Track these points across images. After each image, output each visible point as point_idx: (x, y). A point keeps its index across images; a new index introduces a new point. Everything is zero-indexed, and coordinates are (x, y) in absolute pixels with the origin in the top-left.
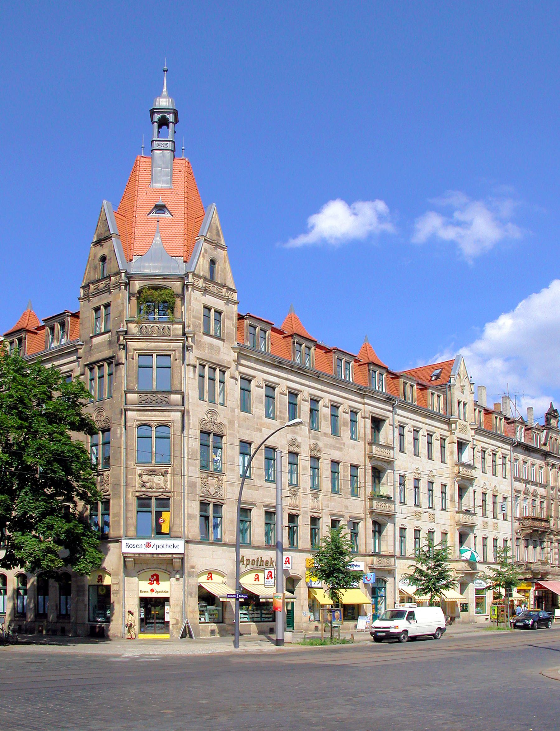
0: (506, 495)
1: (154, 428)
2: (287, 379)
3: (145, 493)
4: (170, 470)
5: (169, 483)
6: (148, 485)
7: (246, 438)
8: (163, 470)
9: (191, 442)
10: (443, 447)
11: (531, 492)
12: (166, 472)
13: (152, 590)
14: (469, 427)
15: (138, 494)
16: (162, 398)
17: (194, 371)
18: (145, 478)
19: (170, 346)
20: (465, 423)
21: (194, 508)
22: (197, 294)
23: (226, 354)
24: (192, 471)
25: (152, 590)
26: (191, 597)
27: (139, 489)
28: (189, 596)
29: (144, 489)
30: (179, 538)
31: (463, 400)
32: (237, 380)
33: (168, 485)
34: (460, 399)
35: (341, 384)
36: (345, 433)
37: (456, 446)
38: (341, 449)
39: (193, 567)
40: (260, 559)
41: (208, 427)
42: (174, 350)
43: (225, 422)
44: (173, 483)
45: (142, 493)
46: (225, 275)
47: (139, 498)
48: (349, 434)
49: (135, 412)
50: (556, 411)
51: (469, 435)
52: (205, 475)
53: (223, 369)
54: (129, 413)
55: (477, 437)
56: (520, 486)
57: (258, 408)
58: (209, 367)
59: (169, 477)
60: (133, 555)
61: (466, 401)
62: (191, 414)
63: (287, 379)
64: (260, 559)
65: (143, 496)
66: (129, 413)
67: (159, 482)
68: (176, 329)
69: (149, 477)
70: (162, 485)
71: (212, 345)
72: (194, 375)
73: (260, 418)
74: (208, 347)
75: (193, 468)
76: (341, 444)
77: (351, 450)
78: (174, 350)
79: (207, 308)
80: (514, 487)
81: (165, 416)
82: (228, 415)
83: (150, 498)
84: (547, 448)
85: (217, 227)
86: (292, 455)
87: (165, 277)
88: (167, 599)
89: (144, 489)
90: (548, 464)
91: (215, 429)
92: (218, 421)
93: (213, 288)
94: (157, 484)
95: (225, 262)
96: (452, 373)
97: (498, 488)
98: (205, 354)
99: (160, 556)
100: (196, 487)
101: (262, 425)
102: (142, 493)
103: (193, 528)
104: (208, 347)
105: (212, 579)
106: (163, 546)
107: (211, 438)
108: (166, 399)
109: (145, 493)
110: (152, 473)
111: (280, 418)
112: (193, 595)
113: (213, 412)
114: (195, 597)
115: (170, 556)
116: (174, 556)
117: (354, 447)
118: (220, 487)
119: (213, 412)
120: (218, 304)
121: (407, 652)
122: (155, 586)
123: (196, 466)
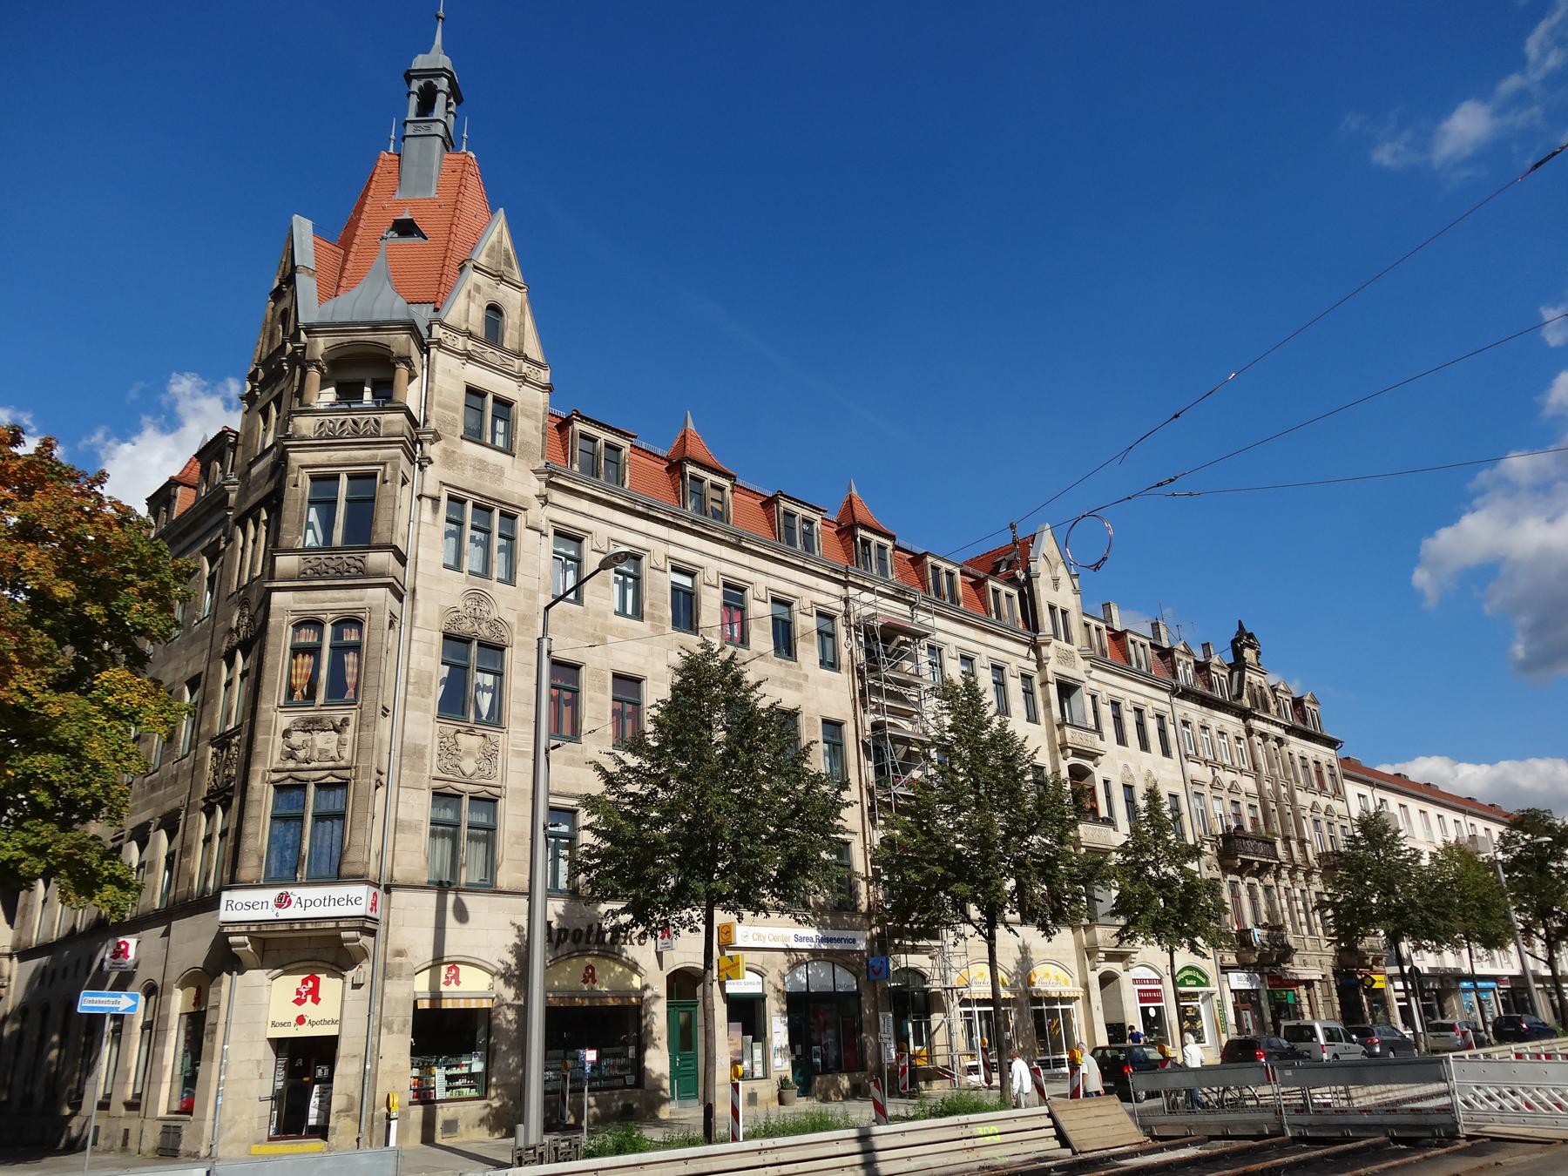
0: (1175, 791)
1: (328, 629)
2: (667, 542)
3: (295, 774)
4: (353, 719)
5: (348, 748)
6: (301, 754)
7: (628, 668)
8: (338, 716)
9: (424, 660)
10: (1028, 693)
11: (1228, 785)
12: (345, 721)
13: (301, 1020)
14: (1077, 656)
15: (275, 777)
16: (351, 561)
17: (435, 509)
18: (297, 738)
19: (376, 456)
20: (1067, 646)
21: (417, 807)
22: (454, 362)
23: (516, 479)
24: (420, 723)
25: (301, 1020)
26: (390, 1030)
27: (281, 766)
28: (384, 1031)
29: (291, 764)
30: (359, 879)
31: (1059, 605)
32: (543, 534)
33: (347, 753)
34: (1054, 602)
35: (715, 530)
36: (808, 653)
37: (1053, 690)
38: (799, 687)
39: (400, 953)
40: (595, 927)
41: (466, 627)
42: (384, 464)
43: (510, 618)
44: (359, 748)
45: (285, 775)
46: (522, 335)
47: (280, 788)
48: (815, 656)
49: (290, 594)
50: (1251, 636)
51: (1078, 670)
52: (450, 729)
53: (511, 510)
54: (276, 596)
55: (1096, 674)
56: (1203, 773)
57: (808, 653)
58: (475, 506)
59: (349, 733)
60: (244, 929)
61: (1066, 607)
62: (419, 596)
63: (667, 542)
64: (595, 927)
65: (289, 782)
66: (276, 596)
67: (327, 747)
68: (391, 422)
69: (307, 736)
70: (334, 753)
71: (482, 461)
72: (435, 518)
73: (601, 614)
74: (461, 463)
75: (418, 714)
76: (798, 676)
77: (823, 691)
78: (384, 464)
79: (474, 393)
80: (1188, 775)
81: (353, 600)
82: (516, 606)
83: (302, 786)
84: (1246, 702)
85: (507, 252)
86: (560, 669)
87: (376, 327)
88: (332, 1041)
89: (291, 764)
90: (1250, 732)
91: (485, 632)
92: (494, 615)
93: (490, 354)
94: (321, 752)
95: (523, 312)
96: (1032, 554)
97: (1155, 776)
98: (466, 478)
99: (309, 926)
100: (422, 757)
101: (609, 629)
102: (285, 775)
103: (413, 854)
104: (461, 463)
105: (458, 983)
106: (323, 902)
107: (470, 654)
108: (359, 564)
109: (295, 774)
110: (310, 726)
111: (652, 618)
112: (395, 1028)
113: (479, 597)
114: (401, 1032)
115: (332, 925)
116: (342, 925)
117: (828, 684)
118: (490, 756)
119: (479, 597)
120: (504, 386)
121: (979, 1141)
122: (308, 1009)
123: (426, 711)
